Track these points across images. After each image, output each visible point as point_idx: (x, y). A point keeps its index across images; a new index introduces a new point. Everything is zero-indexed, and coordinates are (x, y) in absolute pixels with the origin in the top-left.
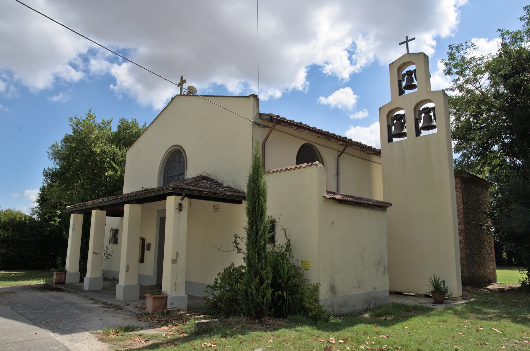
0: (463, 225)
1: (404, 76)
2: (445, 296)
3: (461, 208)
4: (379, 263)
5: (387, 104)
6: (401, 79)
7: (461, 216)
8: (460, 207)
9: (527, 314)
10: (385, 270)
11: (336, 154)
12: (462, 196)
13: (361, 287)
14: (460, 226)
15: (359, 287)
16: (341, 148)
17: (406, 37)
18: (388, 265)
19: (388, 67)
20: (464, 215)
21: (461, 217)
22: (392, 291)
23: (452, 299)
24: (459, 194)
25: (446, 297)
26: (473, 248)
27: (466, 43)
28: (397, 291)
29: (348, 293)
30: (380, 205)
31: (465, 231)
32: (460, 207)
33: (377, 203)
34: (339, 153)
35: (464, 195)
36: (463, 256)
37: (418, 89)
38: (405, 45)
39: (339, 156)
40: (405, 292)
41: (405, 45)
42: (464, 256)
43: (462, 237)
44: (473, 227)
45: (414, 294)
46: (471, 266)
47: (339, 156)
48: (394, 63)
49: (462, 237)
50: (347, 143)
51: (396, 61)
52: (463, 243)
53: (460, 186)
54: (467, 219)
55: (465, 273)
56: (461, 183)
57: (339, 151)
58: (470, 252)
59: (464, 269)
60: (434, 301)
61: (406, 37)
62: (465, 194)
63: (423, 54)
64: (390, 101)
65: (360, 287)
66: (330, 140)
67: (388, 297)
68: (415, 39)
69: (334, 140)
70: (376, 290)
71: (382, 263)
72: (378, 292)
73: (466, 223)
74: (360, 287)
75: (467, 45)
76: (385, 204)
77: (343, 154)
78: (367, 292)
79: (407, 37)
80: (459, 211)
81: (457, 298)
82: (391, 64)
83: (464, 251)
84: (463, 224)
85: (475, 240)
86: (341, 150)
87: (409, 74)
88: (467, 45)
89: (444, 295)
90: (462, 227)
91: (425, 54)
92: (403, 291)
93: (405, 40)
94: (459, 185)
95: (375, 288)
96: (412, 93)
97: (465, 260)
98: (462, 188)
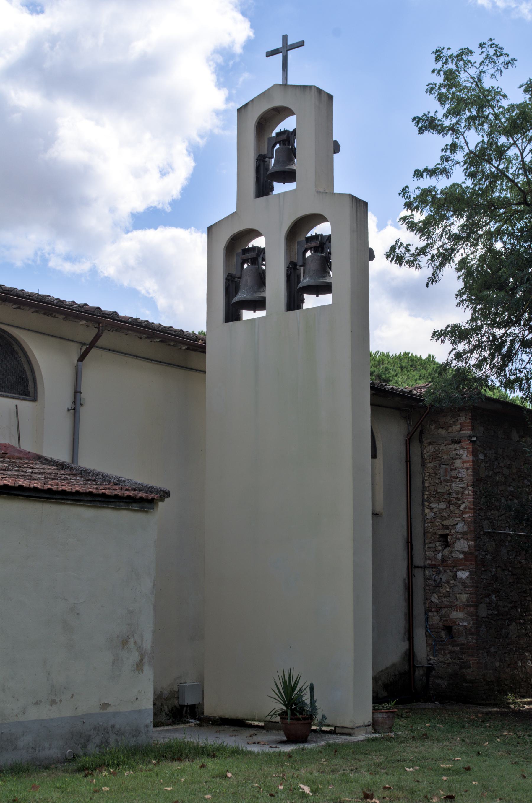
0: (472, 541)
1: (273, 143)
2: (310, 725)
3: (468, 495)
4: (124, 643)
5: (228, 217)
6: (265, 151)
7: (467, 515)
8: (466, 492)
9: (456, 759)
10: (142, 660)
11: (75, 353)
12: (473, 461)
13: (61, 701)
14: (466, 542)
15: (53, 702)
16: (91, 333)
17: (283, 36)
18: (152, 647)
19: (235, 114)
20: (475, 512)
21: (469, 517)
22: (215, 717)
23: (344, 731)
24: (465, 456)
25: (314, 728)
26: (500, 603)
27: (481, 45)
28: (227, 716)
29: (17, 716)
30: (129, 497)
31: (476, 557)
32: (466, 492)
33: (134, 490)
34: (84, 348)
35: (481, 456)
36: (469, 624)
37: (297, 185)
38: (279, 57)
39: (82, 358)
40: (254, 720)
41: (279, 57)
42: (471, 623)
43: (468, 573)
44: (507, 544)
45: (262, 724)
46: (493, 650)
47: (82, 358)
48: (250, 105)
49: (468, 573)
50: (101, 325)
51: (252, 100)
52: (471, 589)
53: (469, 432)
54: (486, 523)
55: (471, 670)
56: (473, 426)
57: (83, 344)
58: (490, 612)
59: (470, 658)
60: (285, 738)
61: (283, 36)
62: (485, 456)
63: (313, 89)
64: (233, 209)
65: (58, 700)
66: (53, 315)
67: (147, 726)
68: (303, 45)
69: (62, 317)
70: (110, 710)
71: (132, 641)
72: (115, 714)
73: (482, 533)
74: (56, 703)
75: (482, 52)
76: (151, 492)
77: (93, 351)
78: (80, 714)
79: (285, 38)
80: (465, 501)
81: (352, 729)
82: (241, 108)
83: (472, 609)
84: (473, 536)
85: (511, 581)
86: (89, 339)
87: (283, 141)
88: (482, 52)
89: (309, 721)
90: (469, 546)
91: (320, 91)
92: (246, 717)
93: (279, 45)
94: (467, 432)
95: (105, 706)
96: (285, 193)
97: (472, 634)
98: (474, 439)
